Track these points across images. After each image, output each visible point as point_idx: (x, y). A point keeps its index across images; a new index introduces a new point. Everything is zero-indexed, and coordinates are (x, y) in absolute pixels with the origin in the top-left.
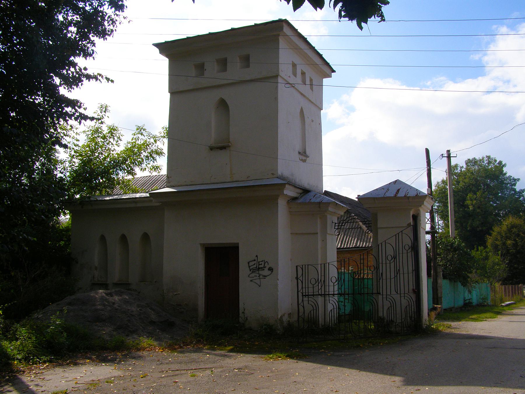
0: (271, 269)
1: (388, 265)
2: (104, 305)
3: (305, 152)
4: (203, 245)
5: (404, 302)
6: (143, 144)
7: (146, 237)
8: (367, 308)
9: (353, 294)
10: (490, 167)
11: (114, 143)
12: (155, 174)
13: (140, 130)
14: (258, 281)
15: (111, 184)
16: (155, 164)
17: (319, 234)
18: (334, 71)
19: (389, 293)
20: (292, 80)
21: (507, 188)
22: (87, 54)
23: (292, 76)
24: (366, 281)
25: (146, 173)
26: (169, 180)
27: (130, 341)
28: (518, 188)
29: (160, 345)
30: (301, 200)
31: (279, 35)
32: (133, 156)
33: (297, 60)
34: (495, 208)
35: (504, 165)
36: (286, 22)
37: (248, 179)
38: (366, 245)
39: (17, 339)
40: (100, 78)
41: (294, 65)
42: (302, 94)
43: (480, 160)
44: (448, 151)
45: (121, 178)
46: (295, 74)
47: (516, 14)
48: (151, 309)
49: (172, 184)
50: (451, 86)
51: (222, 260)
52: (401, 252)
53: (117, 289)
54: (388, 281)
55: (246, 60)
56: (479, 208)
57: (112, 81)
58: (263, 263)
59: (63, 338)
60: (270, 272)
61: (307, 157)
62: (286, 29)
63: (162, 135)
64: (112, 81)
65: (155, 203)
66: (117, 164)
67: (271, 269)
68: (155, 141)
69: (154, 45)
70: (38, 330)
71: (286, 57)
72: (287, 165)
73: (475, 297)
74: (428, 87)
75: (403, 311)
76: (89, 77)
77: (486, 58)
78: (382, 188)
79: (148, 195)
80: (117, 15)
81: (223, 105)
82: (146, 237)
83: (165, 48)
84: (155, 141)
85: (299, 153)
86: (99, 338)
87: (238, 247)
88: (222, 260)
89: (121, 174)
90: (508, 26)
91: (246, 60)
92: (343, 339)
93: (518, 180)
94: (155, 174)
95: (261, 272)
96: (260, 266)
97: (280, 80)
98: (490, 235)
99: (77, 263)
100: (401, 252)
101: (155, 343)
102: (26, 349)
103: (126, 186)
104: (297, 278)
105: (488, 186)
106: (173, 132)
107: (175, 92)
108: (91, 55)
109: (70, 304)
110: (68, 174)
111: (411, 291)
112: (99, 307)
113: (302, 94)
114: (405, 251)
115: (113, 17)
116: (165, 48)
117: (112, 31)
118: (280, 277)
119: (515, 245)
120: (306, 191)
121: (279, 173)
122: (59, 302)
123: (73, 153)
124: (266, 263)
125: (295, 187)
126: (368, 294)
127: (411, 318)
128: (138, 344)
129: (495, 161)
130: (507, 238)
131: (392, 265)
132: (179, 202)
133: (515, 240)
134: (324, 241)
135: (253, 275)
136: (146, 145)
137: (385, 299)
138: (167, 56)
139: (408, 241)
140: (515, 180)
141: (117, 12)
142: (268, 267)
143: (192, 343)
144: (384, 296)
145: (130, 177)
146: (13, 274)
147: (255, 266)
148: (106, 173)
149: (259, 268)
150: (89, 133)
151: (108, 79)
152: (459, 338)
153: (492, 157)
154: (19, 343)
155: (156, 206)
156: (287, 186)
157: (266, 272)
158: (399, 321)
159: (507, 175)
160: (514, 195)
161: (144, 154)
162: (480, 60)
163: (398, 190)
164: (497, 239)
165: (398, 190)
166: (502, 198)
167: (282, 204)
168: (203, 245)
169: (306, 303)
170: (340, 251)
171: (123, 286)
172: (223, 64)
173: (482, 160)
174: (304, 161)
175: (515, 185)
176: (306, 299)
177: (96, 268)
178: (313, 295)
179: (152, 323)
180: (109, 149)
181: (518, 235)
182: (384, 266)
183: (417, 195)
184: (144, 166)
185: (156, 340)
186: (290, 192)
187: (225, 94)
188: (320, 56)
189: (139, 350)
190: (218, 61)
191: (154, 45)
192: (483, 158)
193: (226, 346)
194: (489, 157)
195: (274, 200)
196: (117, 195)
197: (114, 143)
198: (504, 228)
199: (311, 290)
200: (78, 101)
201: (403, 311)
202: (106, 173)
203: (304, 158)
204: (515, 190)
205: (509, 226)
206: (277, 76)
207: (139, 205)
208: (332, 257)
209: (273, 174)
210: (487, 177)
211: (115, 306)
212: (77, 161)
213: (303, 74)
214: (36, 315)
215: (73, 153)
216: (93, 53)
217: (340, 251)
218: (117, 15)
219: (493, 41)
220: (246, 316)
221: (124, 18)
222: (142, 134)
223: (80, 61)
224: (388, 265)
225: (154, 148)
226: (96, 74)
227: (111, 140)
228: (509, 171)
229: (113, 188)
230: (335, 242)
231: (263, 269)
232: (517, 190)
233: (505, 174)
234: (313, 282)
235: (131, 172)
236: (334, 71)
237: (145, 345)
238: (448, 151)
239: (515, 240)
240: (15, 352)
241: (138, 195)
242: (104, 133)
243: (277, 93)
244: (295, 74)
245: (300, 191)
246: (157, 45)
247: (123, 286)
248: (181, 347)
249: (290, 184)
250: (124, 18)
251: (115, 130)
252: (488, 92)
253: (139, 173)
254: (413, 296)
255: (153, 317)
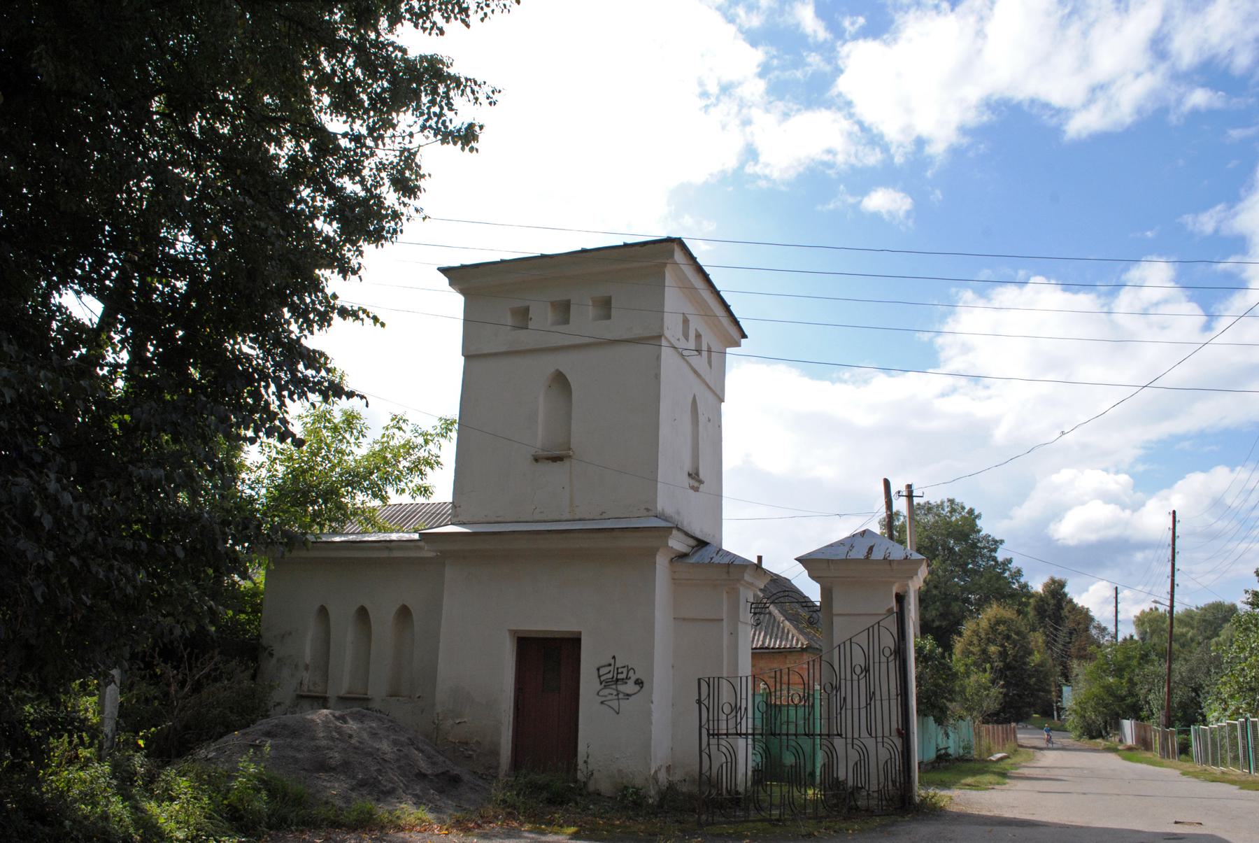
0: (639, 683)
1: (855, 683)
2: (333, 739)
3: (697, 474)
4: (513, 633)
5: (884, 754)
6: (404, 446)
7: (404, 613)
8: (789, 759)
9: (753, 734)
10: (953, 519)
11: (352, 440)
12: (420, 500)
13: (398, 422)
14: (614, 704)
15: (342, 514)
16: (426, 483)
17: (725, 623)
18: (744, 336)
19: (856, 735)
20: (682, 344)
21: (982, 556)
22: (346, 270)
23: (682, 339)
24: (784, 710)
25: (406, 499)
26: (456, 510)
27: (382, 811)
28: (1001, 555)
29: (441, 822)
30: (693, 560)
31: (665, 265)
32: (379, 471)
33: (689, 309)
34: (964, 589)
35: (979, 516)
36: (679, 242)
37: (605, 516)
38: (764, 642)
39: (172, 799)
40: (361, 315)
41: (686, 322)
42: (695, 372)
43: (938, 506)
44: (909, 487)
45: (359, 505)
46: (686, 337)
47: (985, 274)
48: (417, 749)
49: (461, 518)
50: (881, 380)
51: (548, 663)
52: (877, 660)
53: (355, 709)
54: (856, 712)
55: (605, 306)
56: (936, 587)
57: (383, 325)
58: (625, 670)
59: (261, 803)
60: (637, 688)
61: (701, 482)
62: (679, 256)
63: (438, 431)
64: (383, 325)
65: (428, 552)
66: (355, 479)
67: (639, 683)
68: (426, 442)
69: (439, 269)
70: (211, 783)
71: (674, 301)
72: (671, 498)
73: (953, 745)
74: (845, 382)
75: (881, 767)
76: (344, 313)
77: (940, 340)
78: (841, 543)
79: (416, 536)
80: (405, 205)
81: (560, 381)
82: (404, 613)
83: (456, 275)
84: (426, 442)
85: (689, 475)
86: (327, 803)
87: (579, 640)
88: (548, 663)
89: (360, 497)
90: (975, 291)
91: (605, 306)
92: (778, 820)
93: (1002, 542)
94: (420, 500)
95: (621, 688)
96: (620, 676)
97: (664, 342)
98: (960, 634)
99: (271, 655)
100: (877, 660)
101: (430, 817)
102: (192, 821)
103: (369, 518)
104: (699, 702)
105: (951, 550)
106: (472, 424)
107: (474, 355)
108: (355, 272)
109: (268, 734)
110: (263, 491)
111: (894, 732)
112: (324, 743)
113: (695, 372)
114: (883, 659)
115: (397, 207)
116: (456, 275)
117: (395, 231)
118: (655, 698)
119: (1003, 654)
120: (702, 544)
121: (659, 508)
122: (248, 730)
123: (274, 455)
124: (631, 672)
125: (687, 534)
126: (796, 735)
127: (894, 783)
128: (398, 818)
129: (963, 508)
130: (989, 641)
131: (863, 682)
132: (473, 551)
133: (1002, 646)
134: (734, 634)
135: (606, 692)
136: (409, 447)
137: (880, 745)
138: (462, 292)
139: (889, 642)
140: (996, 542)
141: (406, 200)
142: (634, 678)
143: (496, 817)
144: (880, 739)
145: (377, 503)
146: (158, 671)
147: (610, 676)
148: (331, 494)
149: (617, 680)
150: (308, 420)
151: (375, 319)
152: (992, 824)
153: (957, 501)
154: (176, 806)
155: (434, 556)
156: (675, 532)
157: (630, 687)
158: (874, 787)
159: (983, 533)
160: (994, 567)
161: (404, 464)
162: (931, 342)
163: (871, 549)
164: (971, 644)
165: (871, 549)
166: (975, 572)
167: (662, 561)
168: (513, 633)
169: (714, 748)
170: (759, 654)
171: (357, 702)
172: (563, 310)
173: (941, 506)
174: (696, 489)
175: (995, 550)
176: (713, 741)
177: (307, 668)
178: (727, 735)
179: (422, 776)
180: (342, 452)
181: (1008, 637)
182: (849, 683)
183: (906, 558)
184: (402, 485)
185: (431, 810)
186: (677, 543)
187: (563, 362)
188: (726, 307)
189: (401, 829)
190: (553, 304)
191: (439, 269)
192: (942, 503)
193: (561, 826)
194: (952, 501)
195: (649, 555)
196: (353, 533)
197: (352, 440)
198: (984, 624)
199: (723, 726)
200: (322, 354)
201: (881, 767)
202: (331, 494)
203: (696, 484)
204: (995, 559)
205: (993, 620)
206: (659, 337)
207: (396, 554)
208: (745, 666)
209: (648, 510)
210: (949, 535)
211: (353, 741)
212: (280, 469)
213: (698, 336)
214: (202, 753)
215: (274, 455)
216: (359, 268)
217: (759, 654)
218: (405, 205)
219: (951, 313)
220: (590, 768)
221: (417, 210)
222: (400, 428)
223: (332, 281)
224: (855, 683)
225: (422, 454)
226: (355, 308)
227: (347, 435)
228: (988, 527)
229: (344, 522)
230: (750, 638)
231: (624, 681)
232: (1000, 559)
233: (979, 531)
234: (727, 709)
235: (378, 494)
236: (744, 336)
237: (412, 819)
238: (909, 487)
239: (1002, 646)
240: (173, 825)
241: (394, 536)
242: (336, 421)
243: (659, 366)
244: (686, 337)
245: (693, 543)
246: (444, 271)
247: (357, 702)
248: (479, 826)
249: (678, 529)
250: (417, 210)
251: (354, 417)
252: (943, 395)
253: (394, 498)
254: (898, 742)
255: (423, 765)
